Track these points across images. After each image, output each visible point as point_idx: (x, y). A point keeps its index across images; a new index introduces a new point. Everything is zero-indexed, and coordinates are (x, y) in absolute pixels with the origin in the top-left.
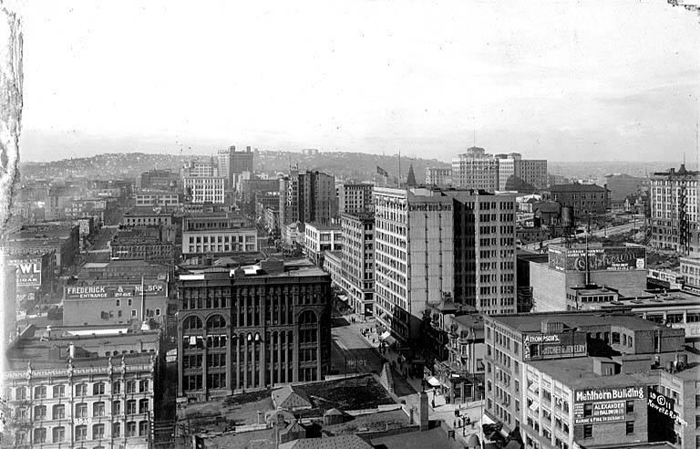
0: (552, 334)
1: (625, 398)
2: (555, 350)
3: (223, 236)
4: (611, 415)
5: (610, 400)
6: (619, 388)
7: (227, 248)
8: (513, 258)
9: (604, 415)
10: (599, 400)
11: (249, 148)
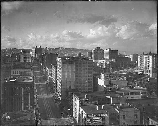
0: (87, 98)
1: (102, 116)
2: (88, 103)
3: (18, 71)
4: (98, 121)
5: (98, 117)
6: (100, 114)
7: (23, 74)
9: (96, 121)
10: (94, 117)
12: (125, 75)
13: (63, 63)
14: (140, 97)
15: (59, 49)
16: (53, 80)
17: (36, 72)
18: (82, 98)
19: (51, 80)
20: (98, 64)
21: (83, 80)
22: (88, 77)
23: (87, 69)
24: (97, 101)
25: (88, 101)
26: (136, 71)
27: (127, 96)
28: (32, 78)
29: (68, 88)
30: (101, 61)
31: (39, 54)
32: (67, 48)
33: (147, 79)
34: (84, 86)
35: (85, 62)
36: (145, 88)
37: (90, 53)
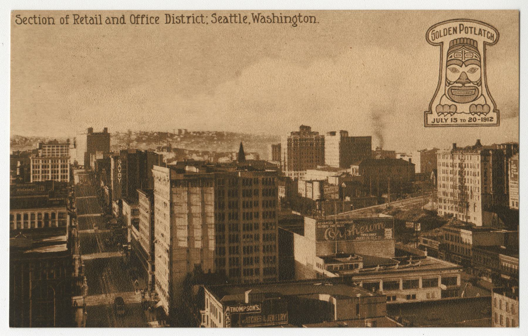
0: (252, 303)
3: (22, 213)
8: (275, 231)
11: (106, 129)
12: (388, 223)
13: (174, 183)
14: (438, 296)
15: (172, 135)
16: (144, 242)
17: (88, 215)
18: (233, 303)
19: (136, 244)
20: (301, 185)
21: (243, 243)
22: (261, 233)
23: (257, 204)
24: (285, 313)
25: (257, 314)
26: (429, 206)
27: (393, 292)
28: (65, 238)
29: (192, 268)
30: (312, 174)
31: (100, 156)
32: (199, 132)
33: (459, 232)
34: (248, 261)
35: (251, 179)
36: (455, 266)
37: (277, 148)
